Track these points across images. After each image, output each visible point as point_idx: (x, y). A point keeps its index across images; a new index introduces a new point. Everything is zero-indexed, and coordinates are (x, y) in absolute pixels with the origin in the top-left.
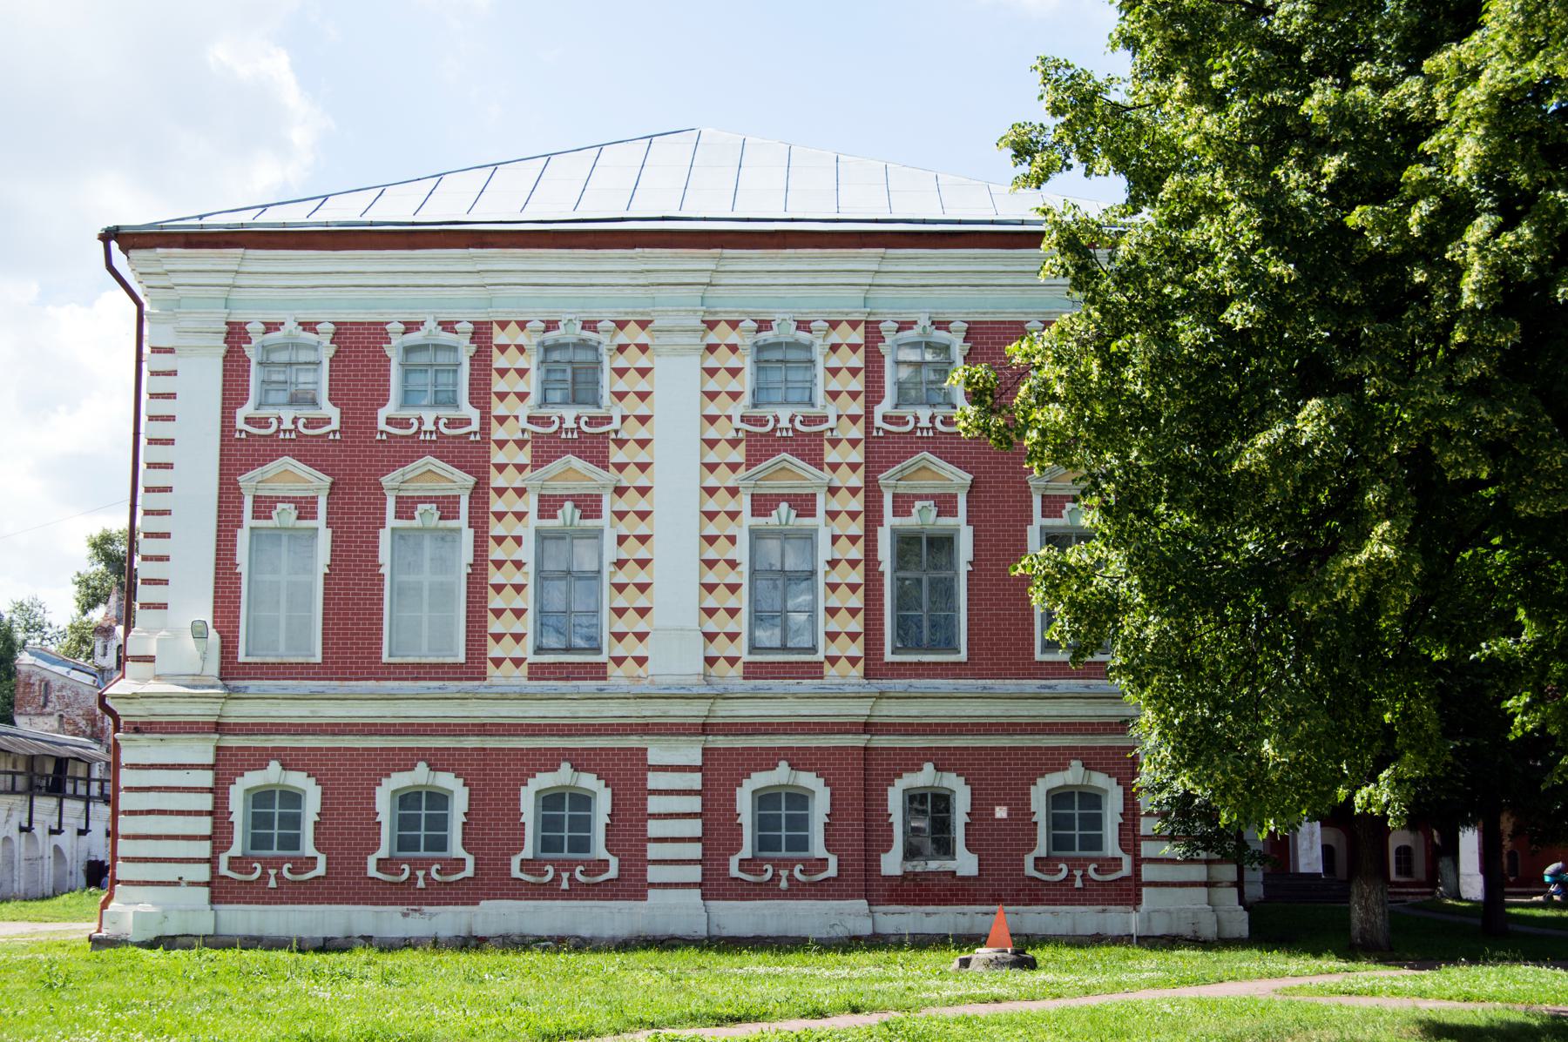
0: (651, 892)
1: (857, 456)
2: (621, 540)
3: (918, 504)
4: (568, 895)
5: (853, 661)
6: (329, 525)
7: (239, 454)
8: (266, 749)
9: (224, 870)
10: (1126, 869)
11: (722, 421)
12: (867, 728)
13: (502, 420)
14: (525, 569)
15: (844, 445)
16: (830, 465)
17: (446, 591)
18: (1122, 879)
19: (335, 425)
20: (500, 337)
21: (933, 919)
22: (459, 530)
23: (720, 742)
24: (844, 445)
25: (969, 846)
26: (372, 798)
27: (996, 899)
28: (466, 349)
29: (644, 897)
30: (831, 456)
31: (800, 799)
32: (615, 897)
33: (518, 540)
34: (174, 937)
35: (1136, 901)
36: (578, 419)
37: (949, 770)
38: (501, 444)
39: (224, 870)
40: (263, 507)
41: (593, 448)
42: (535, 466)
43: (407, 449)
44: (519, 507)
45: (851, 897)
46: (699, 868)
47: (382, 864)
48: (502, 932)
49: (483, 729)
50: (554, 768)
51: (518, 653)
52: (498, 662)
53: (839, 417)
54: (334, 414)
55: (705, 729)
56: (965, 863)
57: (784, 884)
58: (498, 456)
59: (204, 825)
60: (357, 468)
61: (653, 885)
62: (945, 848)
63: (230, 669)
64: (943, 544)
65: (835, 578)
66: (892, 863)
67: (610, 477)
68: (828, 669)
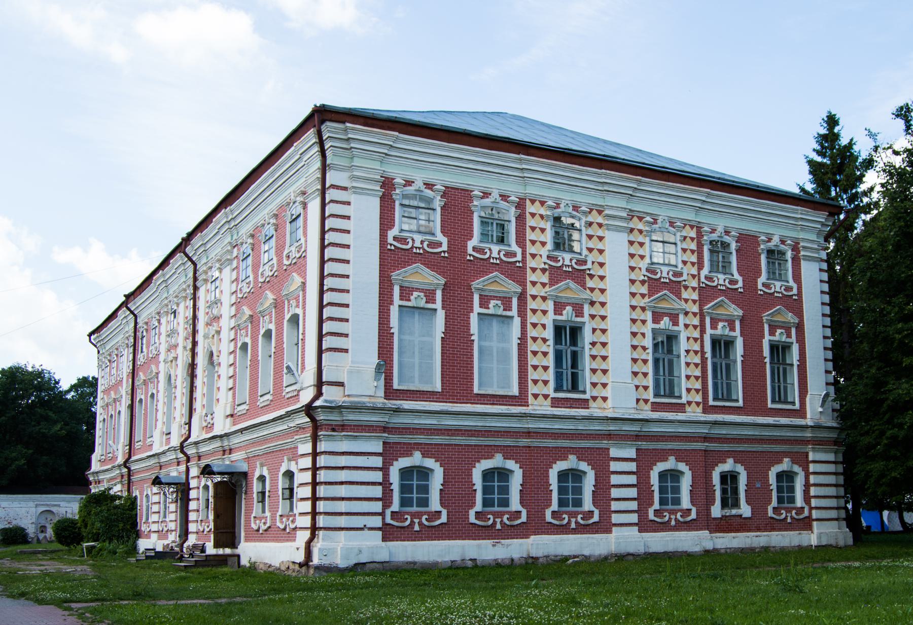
0: (614, 529)
1: (695, 296)
2: (594, 330)
3: (415, 294)
4: (575, 531)
5: (698, 404)
6: (443, 308)
7: (392, 258)
8: (410, 444)
11: (637, 270)
12: (706, 439)
13: (533, 256)
14: (548, 343)
15: (690, 290)
16: (589, 288)
17: (504, 355)
18: (442, 524)
19: (445, 247)
20: (530, 208)
21: (736, 540)
22: (512, 317)
23: (394, 438)
24: (690, 290)
25: (748, 502)
26: (470, 475)
27: (758, 529)
28: (511, 214)
29: (609, 531)
30: (685, 295)
31: (424, 473)
32: (597, 532)
33: (643, 335)
34: (364, 564)
35: (809, 528)
36: (499, 252)
37: (584, 460)
38: (534, 270)
39: (388, 520)
40: (406, 293)
41: (579, 276)
42: (551, 285)
43: (483, 266)
44: (544, 307)
45: (701, 529)
46: (636, 515)
47: (478, 515)
48: (546, 554)
49: (528, 434)
50: (666, 460)
51: (545, 392)
52: (536, 396)
53: (593, 263)
54: (444, 241)
55: (637, 437)
56: (745, 510)
57: (673, 523)
58: (531, 277)
59: (378, 491)
60: (458, 275)
61: (615, 525)
62: (736, 505)
63: (390, 393)
64: (729, 344)
65: (594, 352)
66: (716, 511)
67: (587, 295)
68: (592, 404)
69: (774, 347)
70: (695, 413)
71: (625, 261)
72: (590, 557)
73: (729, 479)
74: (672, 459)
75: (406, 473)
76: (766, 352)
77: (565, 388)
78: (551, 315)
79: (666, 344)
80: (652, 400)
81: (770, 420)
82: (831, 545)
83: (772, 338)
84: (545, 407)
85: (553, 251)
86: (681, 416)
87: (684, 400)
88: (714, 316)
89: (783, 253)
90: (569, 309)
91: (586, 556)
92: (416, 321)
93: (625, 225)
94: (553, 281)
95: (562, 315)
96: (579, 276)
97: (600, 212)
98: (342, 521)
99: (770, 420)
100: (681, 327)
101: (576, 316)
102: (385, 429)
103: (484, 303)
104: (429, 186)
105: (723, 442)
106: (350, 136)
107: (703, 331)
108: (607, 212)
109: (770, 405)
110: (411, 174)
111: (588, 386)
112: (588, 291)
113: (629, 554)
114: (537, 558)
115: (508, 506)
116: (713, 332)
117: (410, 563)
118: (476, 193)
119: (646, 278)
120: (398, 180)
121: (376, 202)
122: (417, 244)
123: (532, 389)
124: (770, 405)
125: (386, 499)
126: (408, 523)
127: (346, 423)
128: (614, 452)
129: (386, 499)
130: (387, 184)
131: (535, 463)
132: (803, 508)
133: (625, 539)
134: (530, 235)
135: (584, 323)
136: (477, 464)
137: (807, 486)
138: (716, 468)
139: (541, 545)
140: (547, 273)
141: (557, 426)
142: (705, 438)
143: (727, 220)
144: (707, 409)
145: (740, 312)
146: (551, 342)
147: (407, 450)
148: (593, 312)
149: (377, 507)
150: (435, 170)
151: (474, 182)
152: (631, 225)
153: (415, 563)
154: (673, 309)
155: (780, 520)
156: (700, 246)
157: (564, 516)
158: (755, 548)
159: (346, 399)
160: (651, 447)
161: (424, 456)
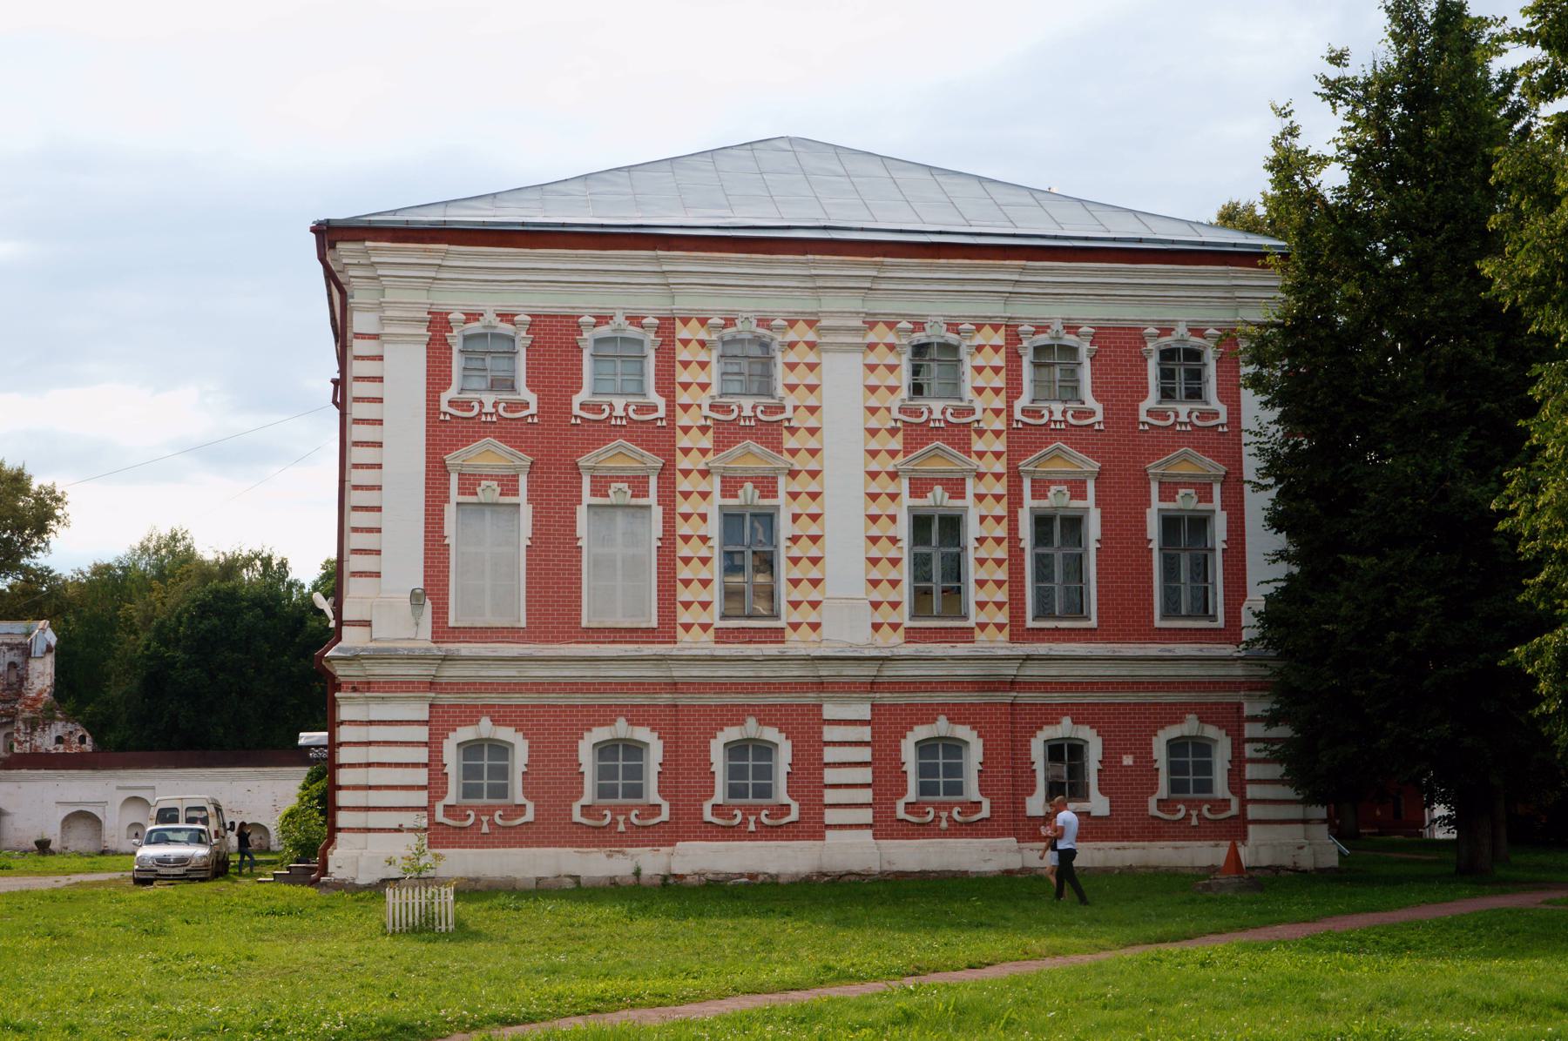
0: (828, 833)
1: (1000, 445)
4: (752, 836)
5: (1000, 627)
6: (1097, 505)
7: (445, 434)
8: (476, 706)
9: (440, 816)
10: (1234, 809)
13: (686, 408)
14: (710, 543)
15: (989, 435)
18: (1231, 818)
20: (682, 332)
23: (446, 699)
24: (989, 435)
31: (955, 747)
36: (754, 408)
38: (686, 430)
39: (440, 816)
40: (469, 483)
41: (769, 432)
42: (717, 451)
43: (600, 431)
49: (674, 686)
51: (894, 619)
52: (687, 627)
53: (796, 408)
55: (873, 685)
58: (683, 441)
59: (421, 776)
60: (555, 453)
63: (441, 631)
64: (1074, 524)
65: (983, 554)
69: (1170, 524)
70: (999, 643)
71: (859, 399)
72: (777, 876)
73: (1066, 753)
74: (942, 720)
75: (471, 749)
76: (1153, 529)
77: (1183, 612)
78: (717, 499)
79: (937, 532)
80: (908, 623)
81: (1153, 649)
82: (1283, 868)
83: (1165, 505)
84: (702, 643)
85: (911, 399)
86: (962, 649)
87: (971, 623)
88: (1037, 476)
89: (1073, 351)
90: (749, 486)
91: (771, 876)
92: (488, 525)
93: (859, 340)
94: (721, 445)
95: (1046, 497)
96: (769, 432)
97: (811, 324)
98: (374, 820)
99: (1153, 649)
100: (970, 499)
101: (762, 496)
102: (432, 685)
103: (600, 487)
104: (1071, 328)
105: (1053, 690)
106: (374, 259)
107: (1015, 500)
108: (824, 323)
109: (1158, 623)
110: (475, 302)
111: (973, 607)
112: (786, 456)
113: (850, 873)
114: (682, 877)
115: (640, 796)
116: (1036, 503)
117: (470, 880)
118: (586, 319)
119: (899, 424)
120: (456, 316)
121: (422, 351)
122: (488, 408)
123: (684, 617)
124: (1158, 623)
125: (436, 786)
126: (930, 818)
127: (372, 679)
128: (830, 711)
129: (436, 786)
130: (439, 324)
131: (684, 729)
132: (1226, 802)
133: (851, 848)
134: (682, 376)
135: (777, 507)
136: (586, 734)
137: (1238, 762)
138: (1160, 733)
139: (697, 858)
140: (710, 433)
141: (723, 672)
142: (1012, 683)
143: (1071, 306)
144: (1018, 633)
145: (1094, 466)
146: (905, 543)
147: (470, 715)
148: (982, 490)
149: (421, 798)
150: (516, 292)
151: (583, 303)
152: (872, 337)
153: (477, 880)
154: (952, 471)
155: (1175, 822)
156: (1014, 357)
157: (737, 812)
158: (1114, 868)
159: (373, 645)
160: (902, 701)
161: (1202, 720)
